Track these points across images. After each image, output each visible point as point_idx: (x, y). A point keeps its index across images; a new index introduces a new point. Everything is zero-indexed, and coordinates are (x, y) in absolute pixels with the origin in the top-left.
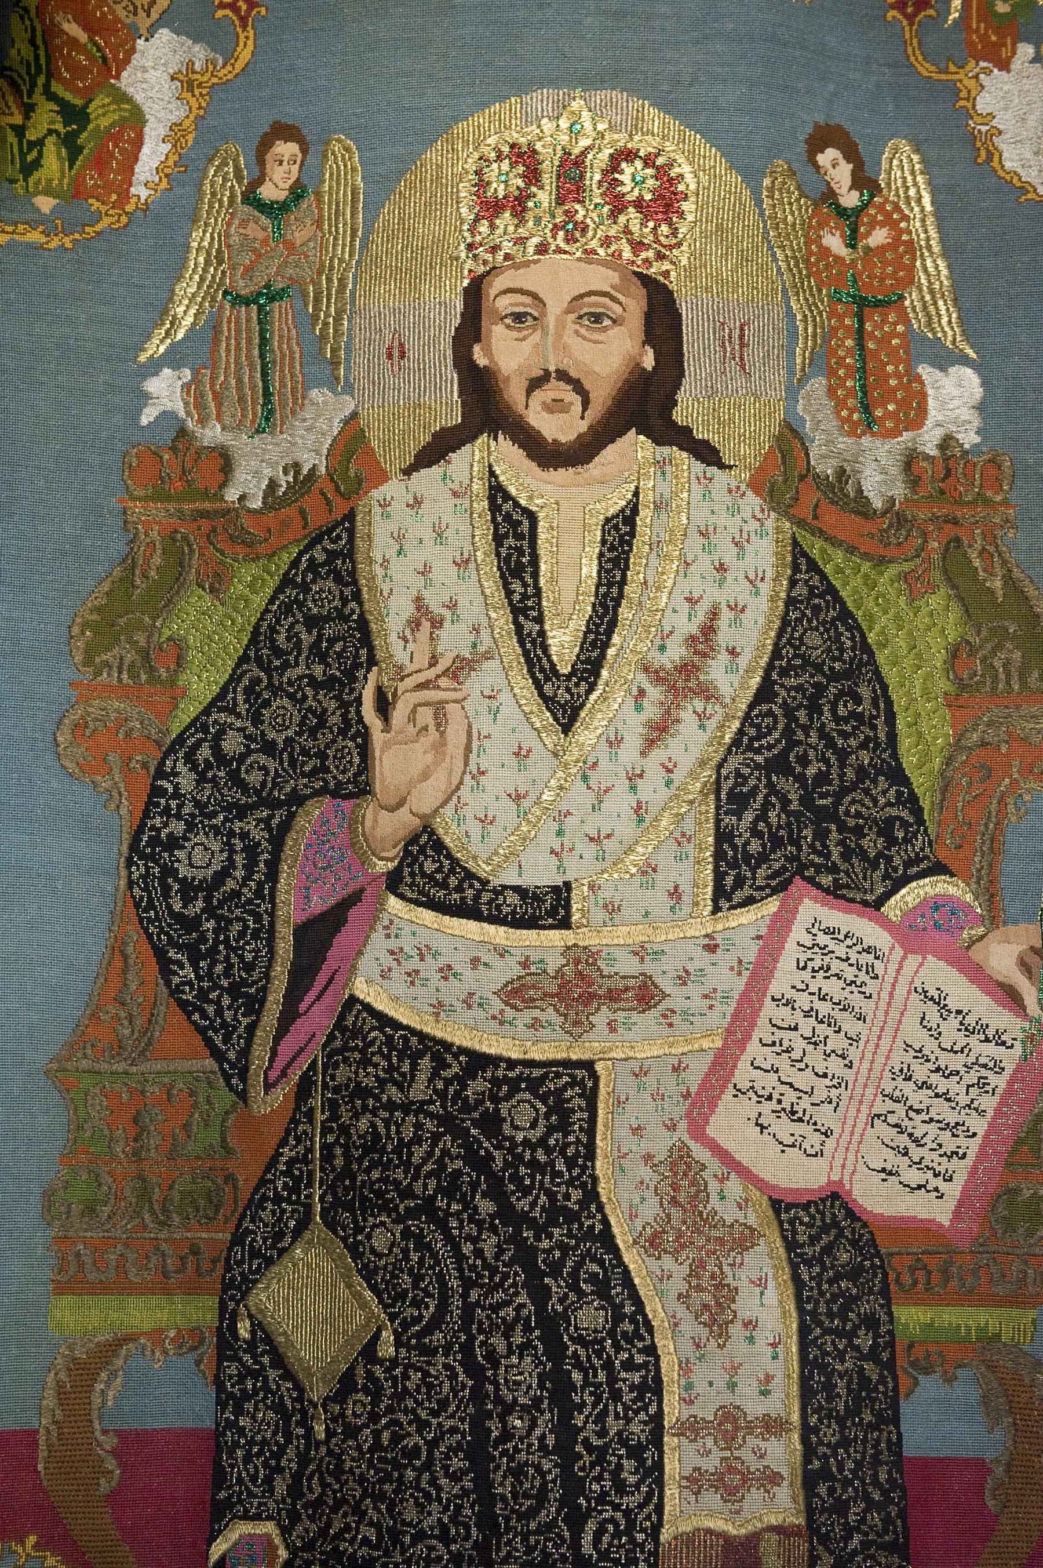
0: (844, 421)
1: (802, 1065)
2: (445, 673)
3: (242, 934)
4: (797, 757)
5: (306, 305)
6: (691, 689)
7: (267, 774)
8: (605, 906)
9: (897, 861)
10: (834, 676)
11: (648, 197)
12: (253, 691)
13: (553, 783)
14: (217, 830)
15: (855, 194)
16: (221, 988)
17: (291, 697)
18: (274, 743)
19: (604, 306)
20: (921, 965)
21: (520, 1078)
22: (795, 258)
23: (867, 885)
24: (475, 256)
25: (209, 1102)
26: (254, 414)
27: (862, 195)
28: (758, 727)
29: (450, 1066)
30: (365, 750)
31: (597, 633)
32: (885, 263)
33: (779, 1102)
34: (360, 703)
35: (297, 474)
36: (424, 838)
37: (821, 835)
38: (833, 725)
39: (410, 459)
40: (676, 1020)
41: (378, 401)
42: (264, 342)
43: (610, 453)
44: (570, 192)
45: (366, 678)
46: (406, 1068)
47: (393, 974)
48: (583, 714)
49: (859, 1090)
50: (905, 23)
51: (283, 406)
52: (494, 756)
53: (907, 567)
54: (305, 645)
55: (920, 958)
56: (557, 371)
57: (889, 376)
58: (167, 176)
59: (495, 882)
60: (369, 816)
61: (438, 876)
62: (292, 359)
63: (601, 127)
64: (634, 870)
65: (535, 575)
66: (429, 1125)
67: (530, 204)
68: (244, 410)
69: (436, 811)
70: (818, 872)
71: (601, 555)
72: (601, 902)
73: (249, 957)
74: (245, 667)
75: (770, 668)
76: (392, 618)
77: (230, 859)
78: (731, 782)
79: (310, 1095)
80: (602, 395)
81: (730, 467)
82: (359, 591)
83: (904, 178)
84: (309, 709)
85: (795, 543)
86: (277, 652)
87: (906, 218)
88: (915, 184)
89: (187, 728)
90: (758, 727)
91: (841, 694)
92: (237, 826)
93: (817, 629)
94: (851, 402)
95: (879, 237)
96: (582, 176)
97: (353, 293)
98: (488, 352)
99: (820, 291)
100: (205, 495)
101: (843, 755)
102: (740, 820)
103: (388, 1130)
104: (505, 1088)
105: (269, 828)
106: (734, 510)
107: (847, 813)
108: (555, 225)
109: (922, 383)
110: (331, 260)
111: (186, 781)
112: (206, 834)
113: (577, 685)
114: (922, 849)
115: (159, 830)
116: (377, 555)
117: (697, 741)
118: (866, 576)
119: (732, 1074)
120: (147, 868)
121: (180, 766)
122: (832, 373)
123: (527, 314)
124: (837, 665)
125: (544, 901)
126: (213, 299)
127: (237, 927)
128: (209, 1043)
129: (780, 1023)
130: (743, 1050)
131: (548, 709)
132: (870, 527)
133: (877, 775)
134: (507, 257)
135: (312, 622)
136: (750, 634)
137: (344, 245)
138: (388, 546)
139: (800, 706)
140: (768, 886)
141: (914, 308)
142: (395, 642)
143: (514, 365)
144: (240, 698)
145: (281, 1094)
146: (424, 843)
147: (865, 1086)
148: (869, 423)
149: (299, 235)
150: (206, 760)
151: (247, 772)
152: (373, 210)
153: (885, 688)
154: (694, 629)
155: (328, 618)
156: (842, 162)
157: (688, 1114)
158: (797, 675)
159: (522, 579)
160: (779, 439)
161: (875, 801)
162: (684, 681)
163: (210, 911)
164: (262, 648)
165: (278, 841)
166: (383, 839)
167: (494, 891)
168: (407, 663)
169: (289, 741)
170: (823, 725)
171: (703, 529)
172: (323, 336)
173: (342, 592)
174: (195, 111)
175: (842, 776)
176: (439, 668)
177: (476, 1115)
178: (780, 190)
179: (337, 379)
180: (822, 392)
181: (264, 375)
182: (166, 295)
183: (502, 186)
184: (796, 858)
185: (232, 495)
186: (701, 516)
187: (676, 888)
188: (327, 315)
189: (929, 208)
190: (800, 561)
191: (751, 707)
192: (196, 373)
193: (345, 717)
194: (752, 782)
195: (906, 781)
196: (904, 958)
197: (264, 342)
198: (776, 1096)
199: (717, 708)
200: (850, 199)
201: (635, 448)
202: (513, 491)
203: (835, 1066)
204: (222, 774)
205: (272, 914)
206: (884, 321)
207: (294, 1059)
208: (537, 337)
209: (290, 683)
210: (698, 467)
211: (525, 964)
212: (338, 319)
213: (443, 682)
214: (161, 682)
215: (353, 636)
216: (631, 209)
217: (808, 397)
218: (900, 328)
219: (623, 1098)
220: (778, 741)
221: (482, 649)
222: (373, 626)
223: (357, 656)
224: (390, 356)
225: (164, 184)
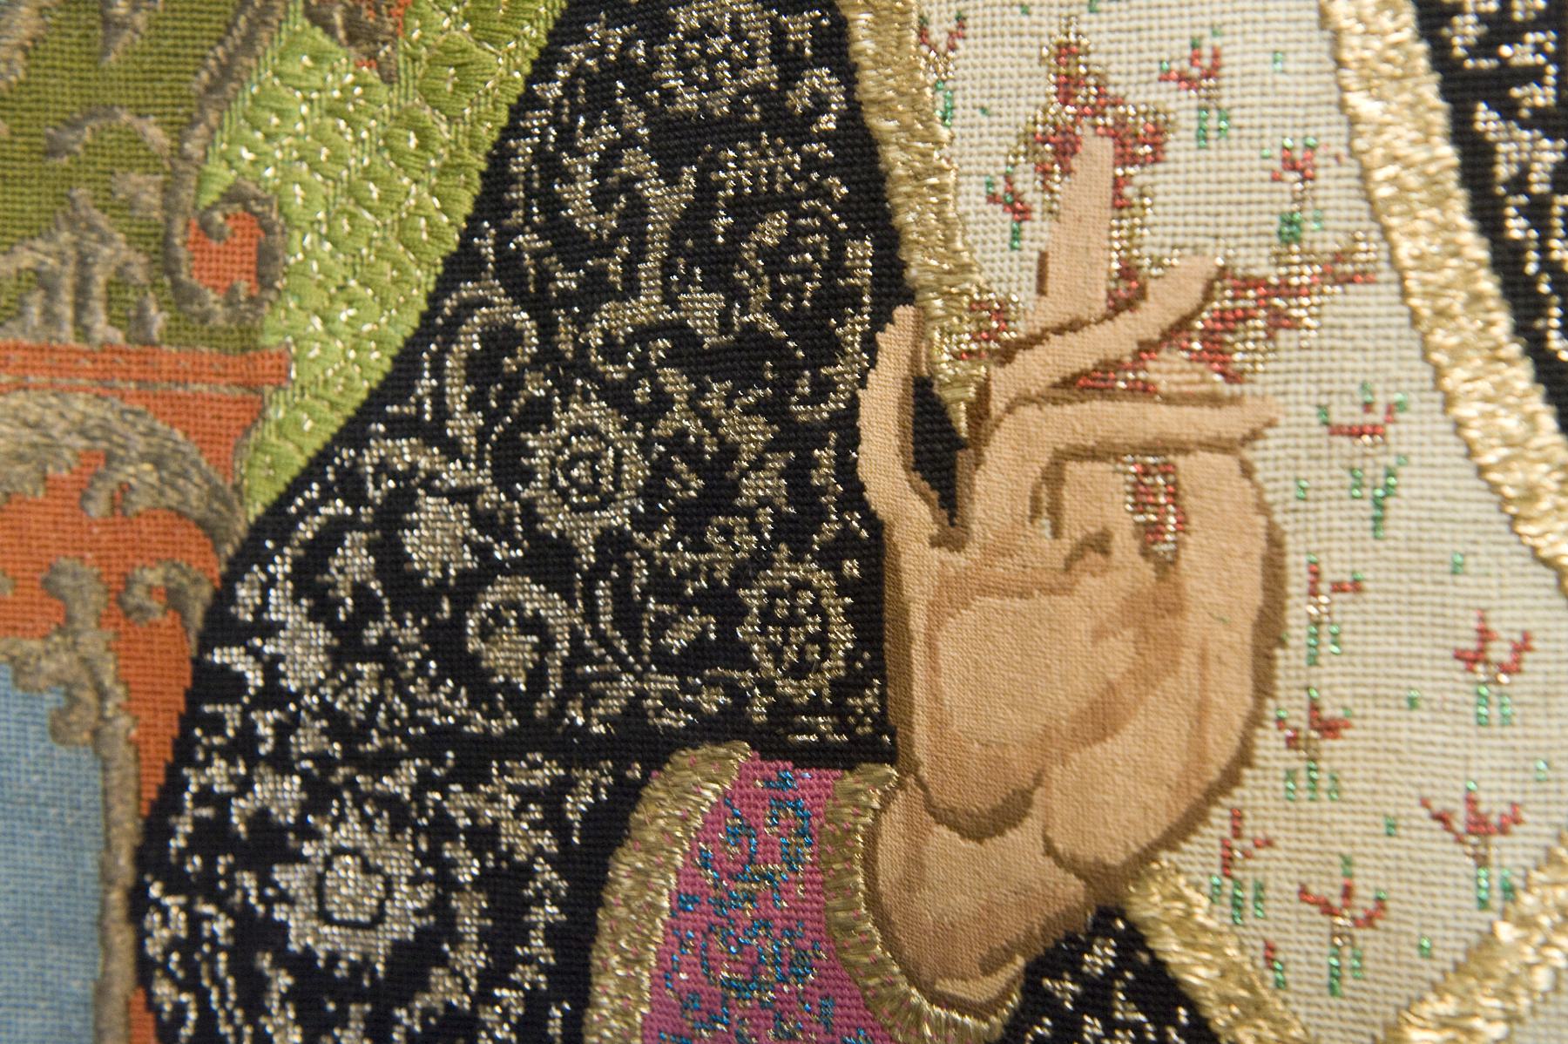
14: (399, 814)
17: (617, 396)
18: (564, 548)
30: (872, 604)
36: (1100, 958)
45: (870, 345)
54: (657, 227)
69: (1147, 856)
74: (468, 289)
77: (439, 906)
82: (841, 27)
84: (678, 441)
86: (568, 243)
89: (297, 486)
92: (459, 804)
105: (555, 821)
111: (304, 653)
112: (367, 822)
115: (223, 803)
120: (195, 921)
121: (281, 607)
135: (678, 142)
144: (458, 395)
150: (359, 590)
151: (485, 633)
155: (731, 129)
164: (521, 235)
165: (587, 868)
166: (946, 933)
169: (612, 544)
173: (779, 33)
176: (1151, 318)
193: (797, 474)
204: (411, 634)
214: (211, 337)
215: (816, 191)
222: (895, 158)
223: (836, 265)
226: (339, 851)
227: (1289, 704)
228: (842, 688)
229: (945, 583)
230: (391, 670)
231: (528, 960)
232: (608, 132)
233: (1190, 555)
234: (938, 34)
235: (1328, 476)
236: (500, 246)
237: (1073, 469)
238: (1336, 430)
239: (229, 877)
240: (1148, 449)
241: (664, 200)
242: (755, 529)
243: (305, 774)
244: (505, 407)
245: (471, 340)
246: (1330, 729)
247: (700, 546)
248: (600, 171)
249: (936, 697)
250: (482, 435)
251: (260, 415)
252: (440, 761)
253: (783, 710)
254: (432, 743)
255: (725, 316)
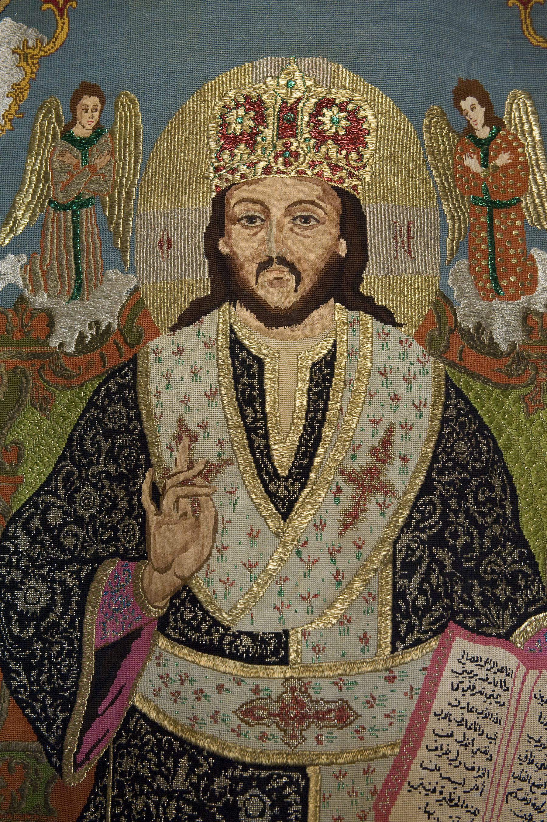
0: (480, 289)
1: (457, 763)
2: (199, 474)
3: (59, 654)
4: (450, 533)
5: (104, 211)
6: (374, 487)
7: (78, 539)
8: (314, 648)
9: (520, 603)
10: (475, 473)
11: (342, 133)
12: (69, 481)
13: (276, 556)
14: (44, 578)
15: (487, 129)
16: (45, 691)
17: (94, 486)
18: (82, 518)
19: (311, 211)
20: (539, 677)
21: (251, 778)
22: (445, 175)
23: (500, 623)
24: (220, 176)
25: (36, 773)
26: (70, 286)
27: (491, 129)
28: (423, 512)
29: (201, 766)
30: (143, 527)
31: (307, 446)
32: (508, 177)
33: (441, 793)
34: (140, 494)
35: (98, 329)
36: (184, 595)
37: (467, 589)
38: (475, 508)
39: (175, 320)
40: (366, 734)
41: (153, 278)
42: (76, 236)
43: (316, 316)
44: (287, 130)
45: (144, 476)
46: (170, 764)
47: (162, 693)
48: (297, 506)
49: (497, 776)
50: (521, 8)
51: (89, 281)
52: (233, 536)
53: (524, 391)
55: (537, 672)
56: (278, 257)
57: (511, 257)
58: (10, 120)
59: (234, 629)
60: (146, 576)
61: (194, 623)
62: (95, 248)
63: (308, 83)
64: (334, 621)
65: (263, 404)
66: (187, 809)
67: (259, 139)
68: (63, 283)
69: (193, 574)
70: (465, 616)
71: (310, 390)
72: (311, 645)
73: (64, 670)
74: (63, 463)
75: (430, 469)
76: (164, 432)
77: (52, 599)
78: (403, 554)
79: (105, 776)
80: (310, 275)
81: (401, 325)
82: (140, 413)
83: (521, 118)
84: (106, 495)
85: (447, 376)
87: (522, 145)
88: (528, 121)
90: (423, 512)
91: (480, 485)
92: (58, 575)
93: (463, 439)
94: (485, 276)
95: (503, 159)
96: (295, 119)
97: (136, 202)
98: (229, 244)
99: (463, 198)
100: (37, 342)
101: (482, 529)
102: (410, 582)
103: (158, 810)
104: (241, 785)
105: (79, 578)
106: (404, 356)
107: (485, 572)
108: (277, 154)
109: (534, 261)
110: (121, 179)
111: (23, 543)
112: (36, 580)
113: (293, 484)
114: (538, 593)
116: (152, 388)
117: (379, 524)
118: (497, 400)
119: (406, 775)
122: (471, 256)
123: (256, 217)
124: (477, 465)
125: (270, 644)
126: (42, 206)
127: (57, 648)
128: (37, 730)
129: (440, 733)
130: (414, 756)
131: (273, 502)
132: (499, 364)
133: (505, 541)
134: (243, 176)
135: (109, 434)
136: (416, 446)
137: (130, 168)
138: (160, 382)
139: (452, 496)
140: (431, 630)
141: (528, 208)
142: (166, 452)
143: (247, 254)
144: (60, 485)
145: (85, 773)
146: (184, 597)
147: (501, 772)
148: (497, 290)
149: (99, 161)
150: (37, 528)
151: (64, 537)
152: (149, 142)
153: (510, 478)
154: (376, 442)
155: (119, 432)
156: (478, 106)
157: (376, 806)
158: (449, 474)
159: (253, 407)
160: (435, 304)
161: (504, 560)
162: (369, 481)
163: (38, 635)
164: (75, 451)
165: (85, 588)
166: (156, 593)
167: (234, 635)
168: (173, 466)
169: (92, 517)
170: (468, 508)
171: (382, 370)
172: (116, 233)
173: (128, 414)
174: (29, 75)
175: (481, 544)
176: (195, 471)
177: (220, 804)
178: (435, 127)
179: (125, 263)
180: (465, 270)
181: (76, 259)
182: (10, 204)
183: (239, 126)
184: (450, 608)
185: (54, 343)
186: (381, 361)
187: (365, 634)
188: (119, 218)
189: (538, 138)
190: (451, 391)
191: (417, 498)
192: (30, 258)
193: (130, 502)
194: (418, 553)
195: (526, 545)
196: (526, 674)
197: (76, 236)
198: (438, 789)
199: (393, 500)
200: (484, 133)
201: (334, 312)
202: (247, 343)
203: (480, 761)
204: (47, 538)
205: (80, 640)
206: (507, 218)
207: (94, 747)
208: (263, 233)
209: (93, 476)
210: (379, 325)
211: (256, 691)
212: (126, 221)
213: (198, 481)
214: (6, 473)
216: (330, 142)
217: (455, 274)
218: (518, 223)
219: (327, 795)
220: (437, 523)
221: (225, 457)
223: (138, 460)
224: (161, 247)
225: (8, 126)
226: (30, 587)
227: (218, 544)
228: (138, 545)
229: (157, 522)
230: (43, 546)
231: (71, 609)
232: (94, 431)
233: (201, 516)
234: (158, 416)
235: (226, 501)
236: (71, 454)
237: (181, 500)
238: (227, 492)
239: (4, 594)
240: (194, 496)
241: (105, 446)
242: (121, 513)
243: (23, 570)
244: (70, 488)
245: (64, 474)
246: (226, 548)
247: (110, 517)
248: (92, 439)
249: (155, 545)
250: (65, 494)
251: (16, 490)
252: (53, 566)
253: (126, 550)
254: (52, 562)
255: (116, 469)
